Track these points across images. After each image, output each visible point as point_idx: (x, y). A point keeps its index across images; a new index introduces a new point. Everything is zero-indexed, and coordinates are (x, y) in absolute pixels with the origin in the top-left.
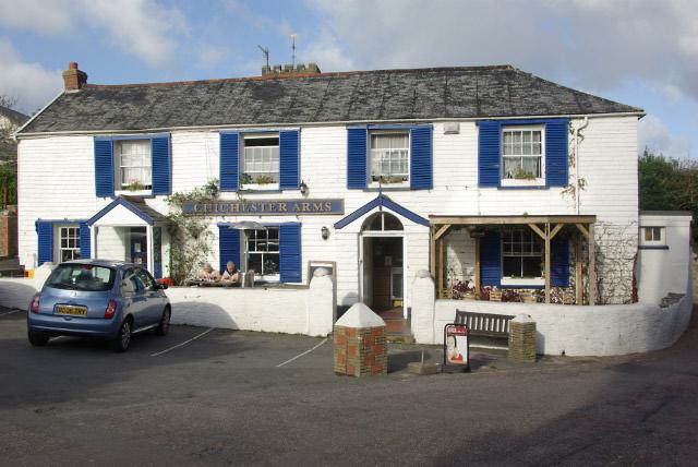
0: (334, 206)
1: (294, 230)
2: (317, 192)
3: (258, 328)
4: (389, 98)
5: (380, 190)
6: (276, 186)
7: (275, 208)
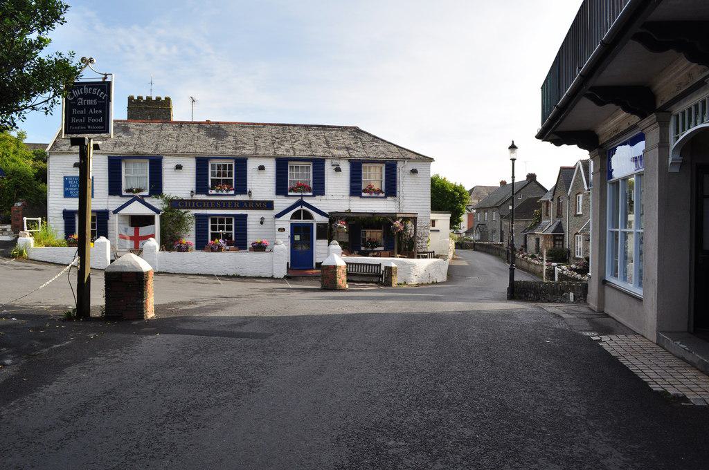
0: (268, 205)
1: (242, 220)
2: (257, 196)
4: (294, 142)
5: (302, 196)
6: (232, 192)
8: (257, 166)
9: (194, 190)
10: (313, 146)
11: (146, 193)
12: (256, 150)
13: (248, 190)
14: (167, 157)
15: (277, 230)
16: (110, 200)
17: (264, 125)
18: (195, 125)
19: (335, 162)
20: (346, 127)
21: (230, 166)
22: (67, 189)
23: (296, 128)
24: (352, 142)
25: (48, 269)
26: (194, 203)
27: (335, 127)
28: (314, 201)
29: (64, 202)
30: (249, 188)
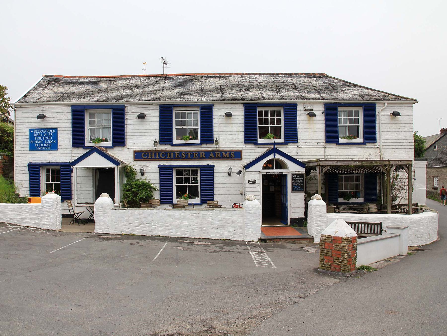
3: (300, 167)
6: (197, 141)
7: (198, 155)
8: (136, 115)
9: (158, 140)
10: (282, 91)
11: (110, 144)
12: (222, 96)
13: (215, 139)
14: (129, 107)
15: (247, 182)
16: (73, 152)
17: (230, 75)
18: (144, 78)
19: (308, 106)
20: (314, 75)
21: (279, 114)
22: (32, 142)
23: (262, 76)
24: (322, 87)
25: (114, 231)
26: (157, 154)
27: (302, 74)
28: (289, 150)
29: (30, 155)
30: (216, 135)
